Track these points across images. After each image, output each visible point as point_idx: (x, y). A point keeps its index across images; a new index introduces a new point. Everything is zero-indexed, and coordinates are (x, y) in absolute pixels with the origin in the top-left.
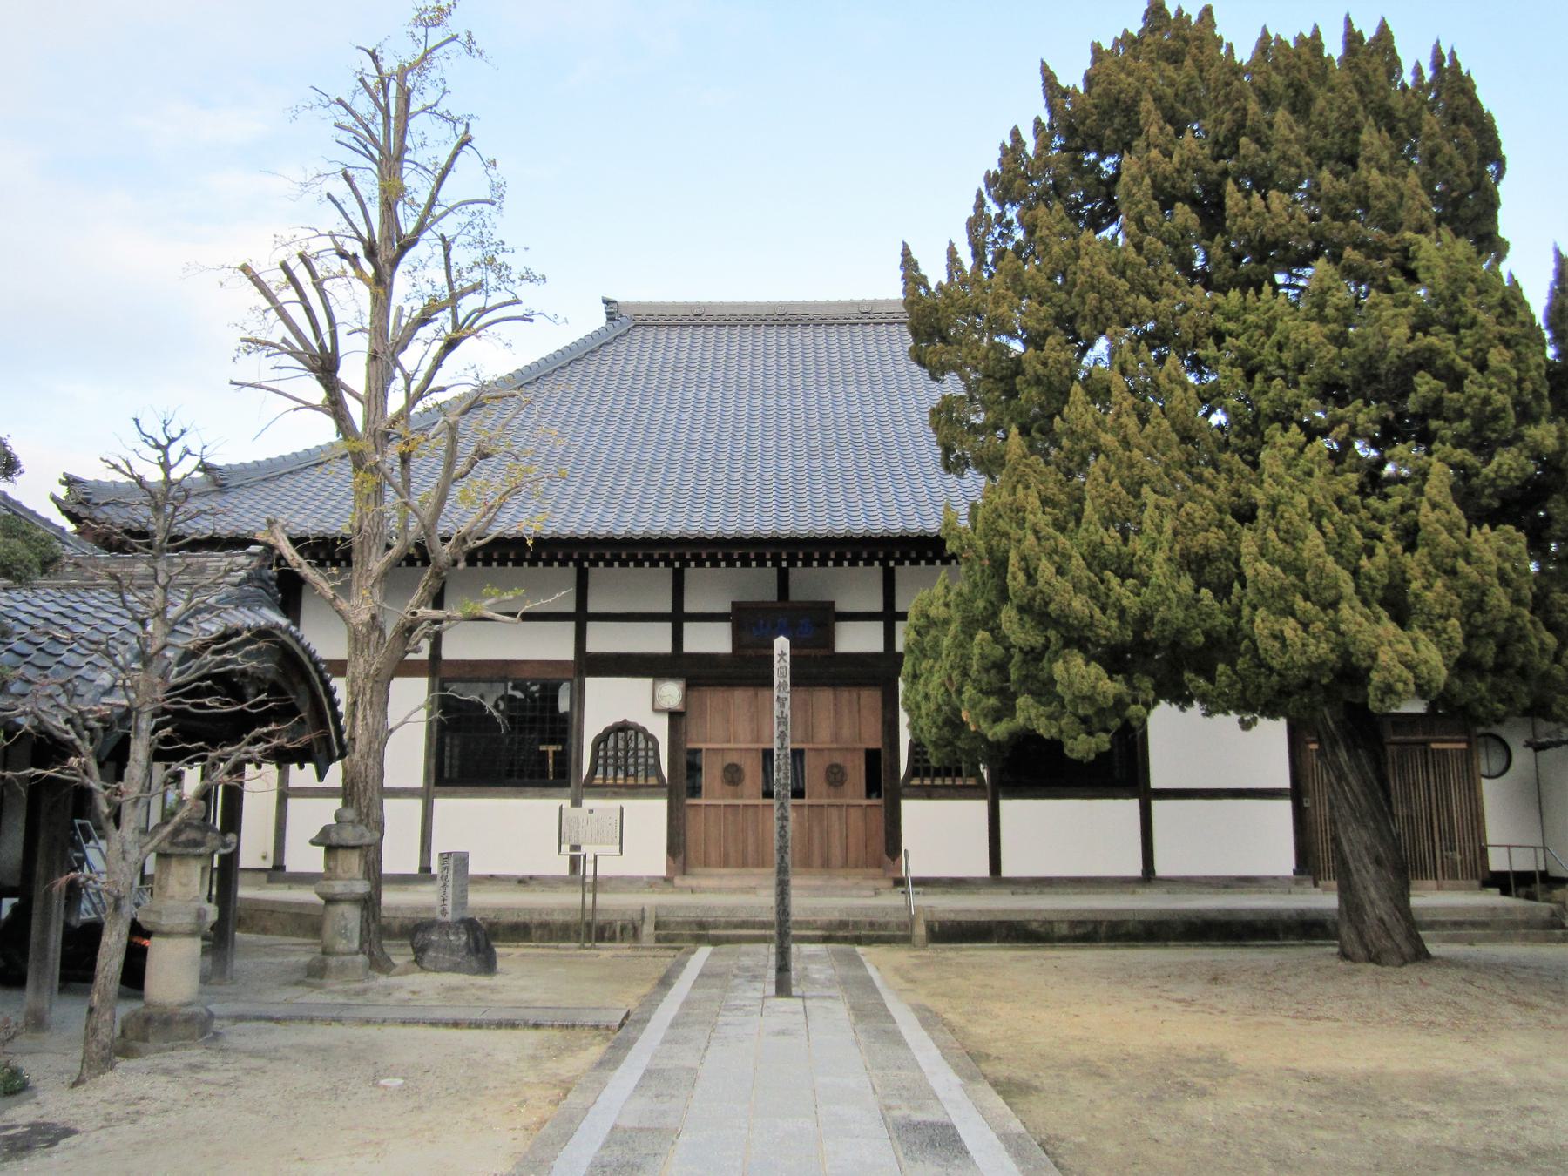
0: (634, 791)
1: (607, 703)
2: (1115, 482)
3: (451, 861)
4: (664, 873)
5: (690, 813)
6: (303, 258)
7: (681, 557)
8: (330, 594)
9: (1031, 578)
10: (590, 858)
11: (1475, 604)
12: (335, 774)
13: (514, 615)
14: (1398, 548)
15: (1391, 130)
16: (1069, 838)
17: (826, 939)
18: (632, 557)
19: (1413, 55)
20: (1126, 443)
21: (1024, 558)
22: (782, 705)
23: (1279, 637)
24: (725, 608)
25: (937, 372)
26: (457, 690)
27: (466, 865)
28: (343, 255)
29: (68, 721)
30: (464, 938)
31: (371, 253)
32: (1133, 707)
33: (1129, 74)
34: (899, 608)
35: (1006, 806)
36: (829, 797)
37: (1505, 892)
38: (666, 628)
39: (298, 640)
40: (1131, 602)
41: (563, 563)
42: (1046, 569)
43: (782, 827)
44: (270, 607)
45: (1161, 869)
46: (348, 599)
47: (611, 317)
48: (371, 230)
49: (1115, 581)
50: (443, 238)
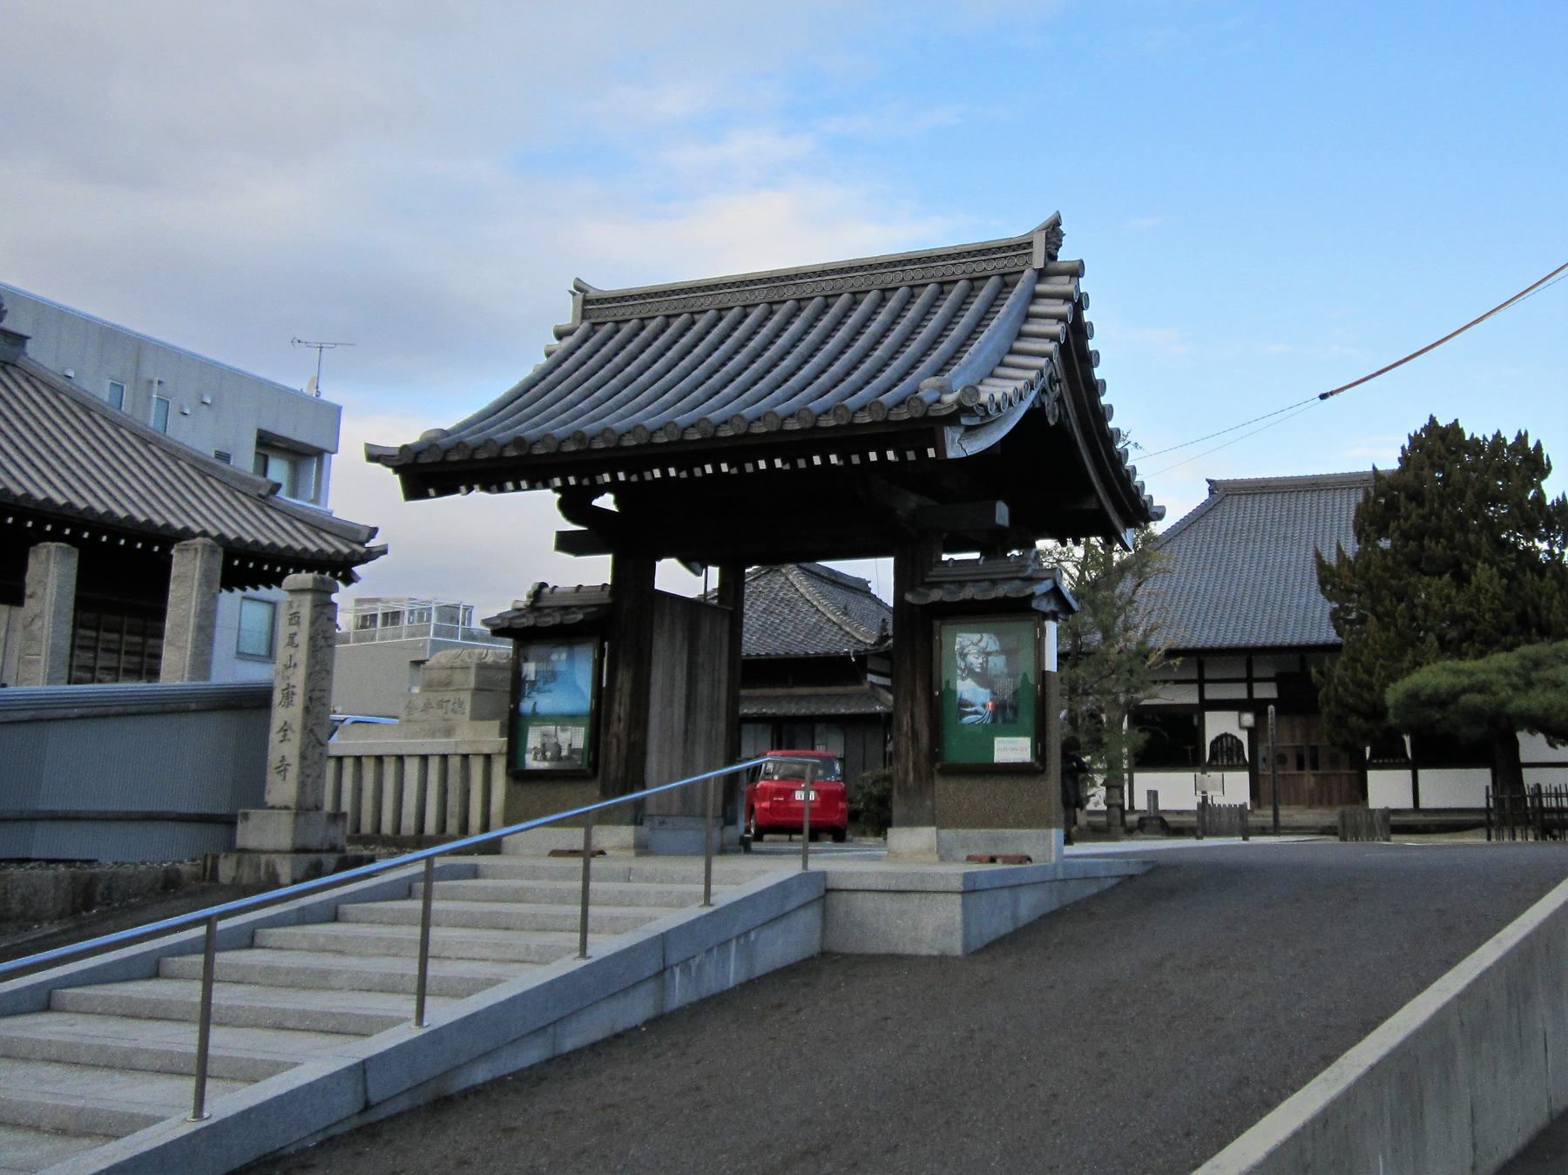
1: (1217, 725)
24: (1272, 675)
35: (1422, 773)
45: (1423, 804)
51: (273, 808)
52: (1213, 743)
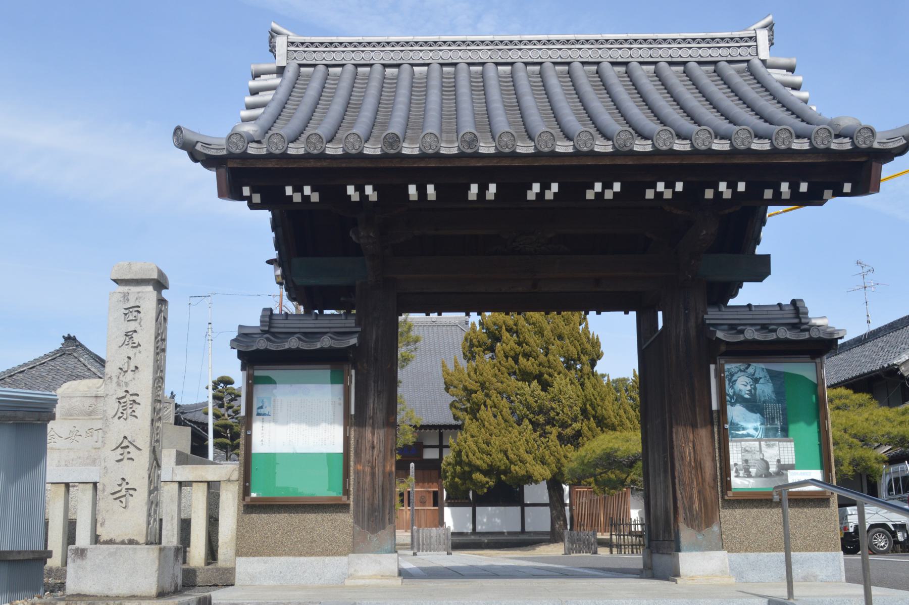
9: (467, 456)
34: (445, 443)
35: (478, 509)
40: (488, 461)
42: (470, 455)
45: (527, 529)
51: (110, 542)
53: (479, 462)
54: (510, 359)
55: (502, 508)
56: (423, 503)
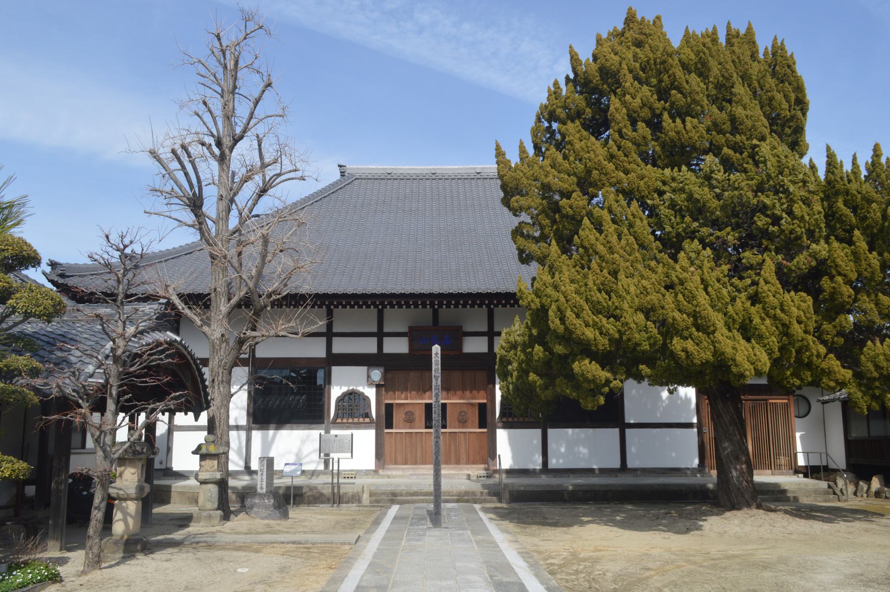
0: (358, 426)
2: (605, 271)
3: (265, 462)
4: (373, 468)
5: (387, 437)
6: (184, 147)
7: (382, 303)
8: (199, 323)
9: (562, 320)
10: (336, 460)
11: (785, 330)
12: (204, 417)
13: (296, 334)
14: (749, 303)
15: (749, 86)
16: (579, 449)
17: (458, 501)
18: (357, 303)
19: (763, 44)
20: (611, 250)
21: (559, 310)
22: (437, 380)
23: (685, 350)
24: (405, 329)
25: (515, 212)
26: (263, 373)
27: (273, 464)
28: (203, 144)
29: (74, 391)
30: (272, 501)
31: (219, 144)
32: (615, 382)
33: (616, 54)
34: (496, 329)
35: (551, 432)
36: (459, 428)
37: (806, 476)
38: (374, 341)
39: (186, 348)
41: (320, 307)
43: (437, 442)
44: (171, 331)
45: (630, 464)
46: (209, 325)
47: (343, 174)
48: (218, 131)
49: (604, 320)
50: (258, 136)
52: (340, 400)
53: (590, 333)
54: (641, 125)
55: (590, 431)
56: (463, 422)
